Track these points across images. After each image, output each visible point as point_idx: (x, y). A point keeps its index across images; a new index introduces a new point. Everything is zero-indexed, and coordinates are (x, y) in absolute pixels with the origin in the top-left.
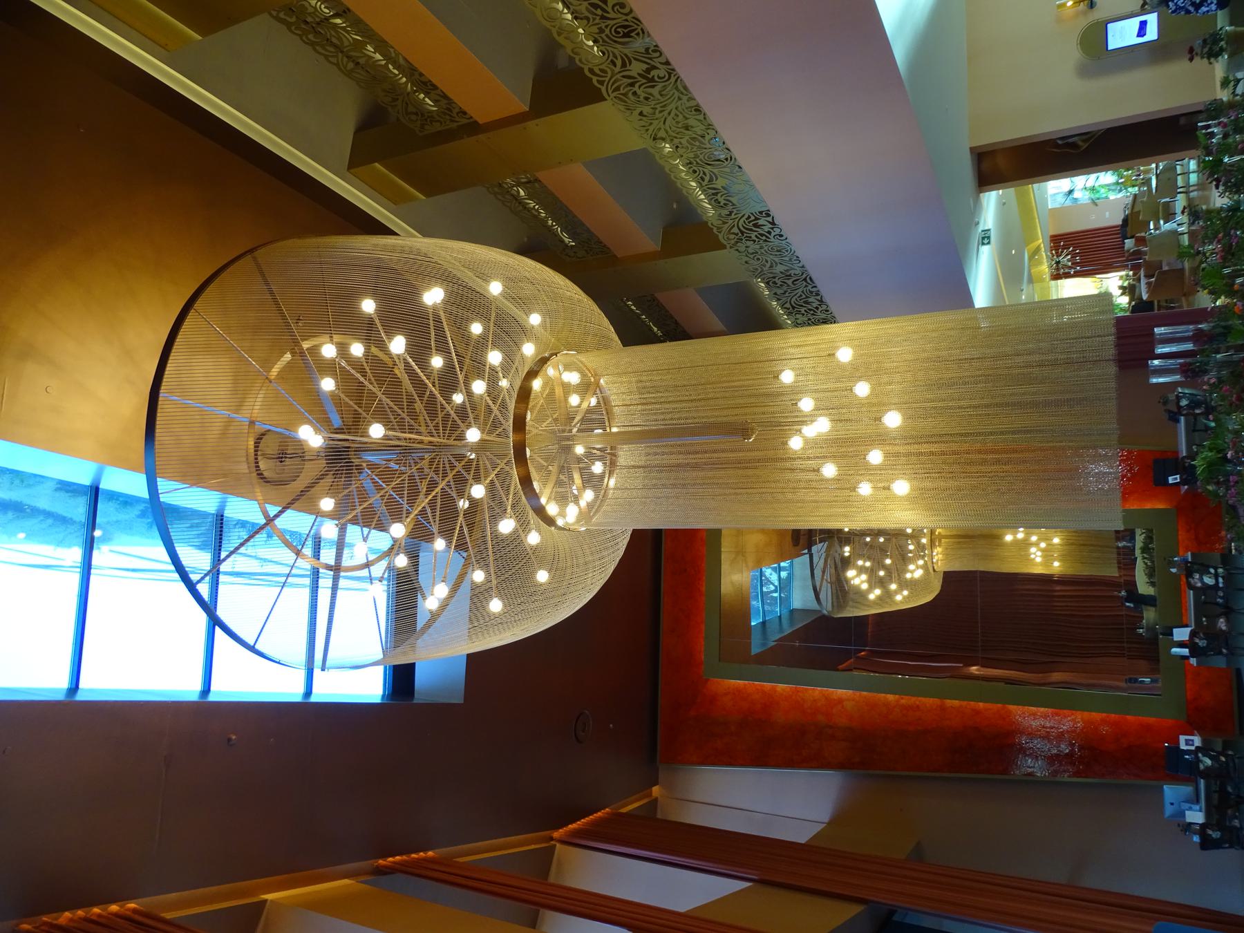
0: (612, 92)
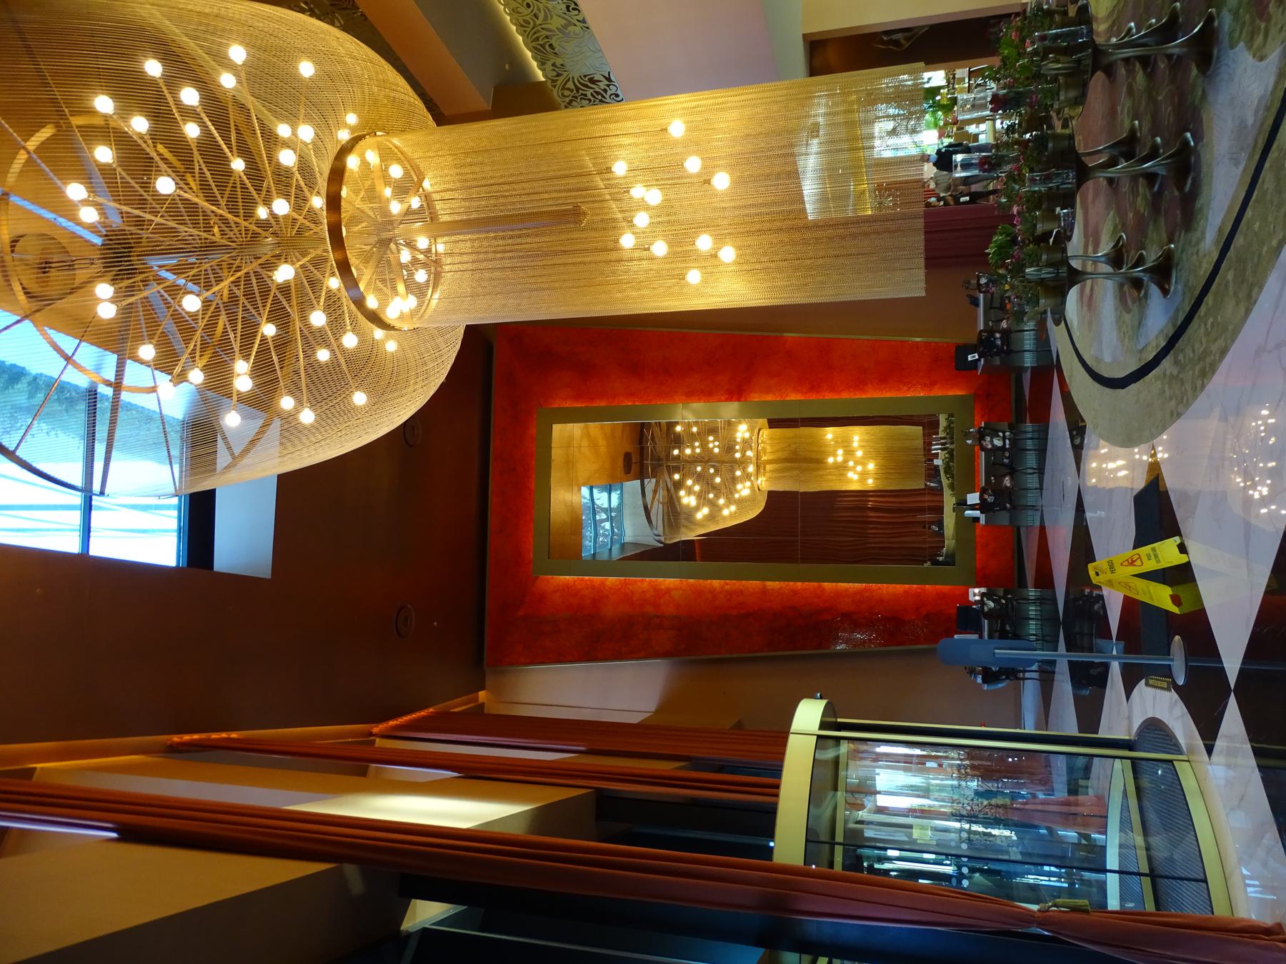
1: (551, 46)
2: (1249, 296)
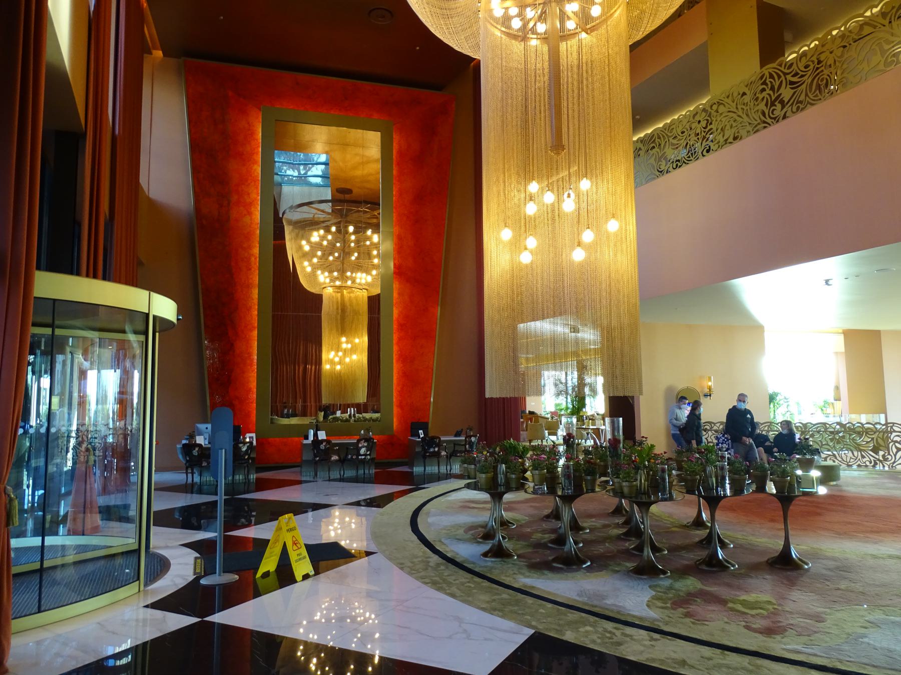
0: (769, 72)
1: (654, 147)
2: (495, 610)
